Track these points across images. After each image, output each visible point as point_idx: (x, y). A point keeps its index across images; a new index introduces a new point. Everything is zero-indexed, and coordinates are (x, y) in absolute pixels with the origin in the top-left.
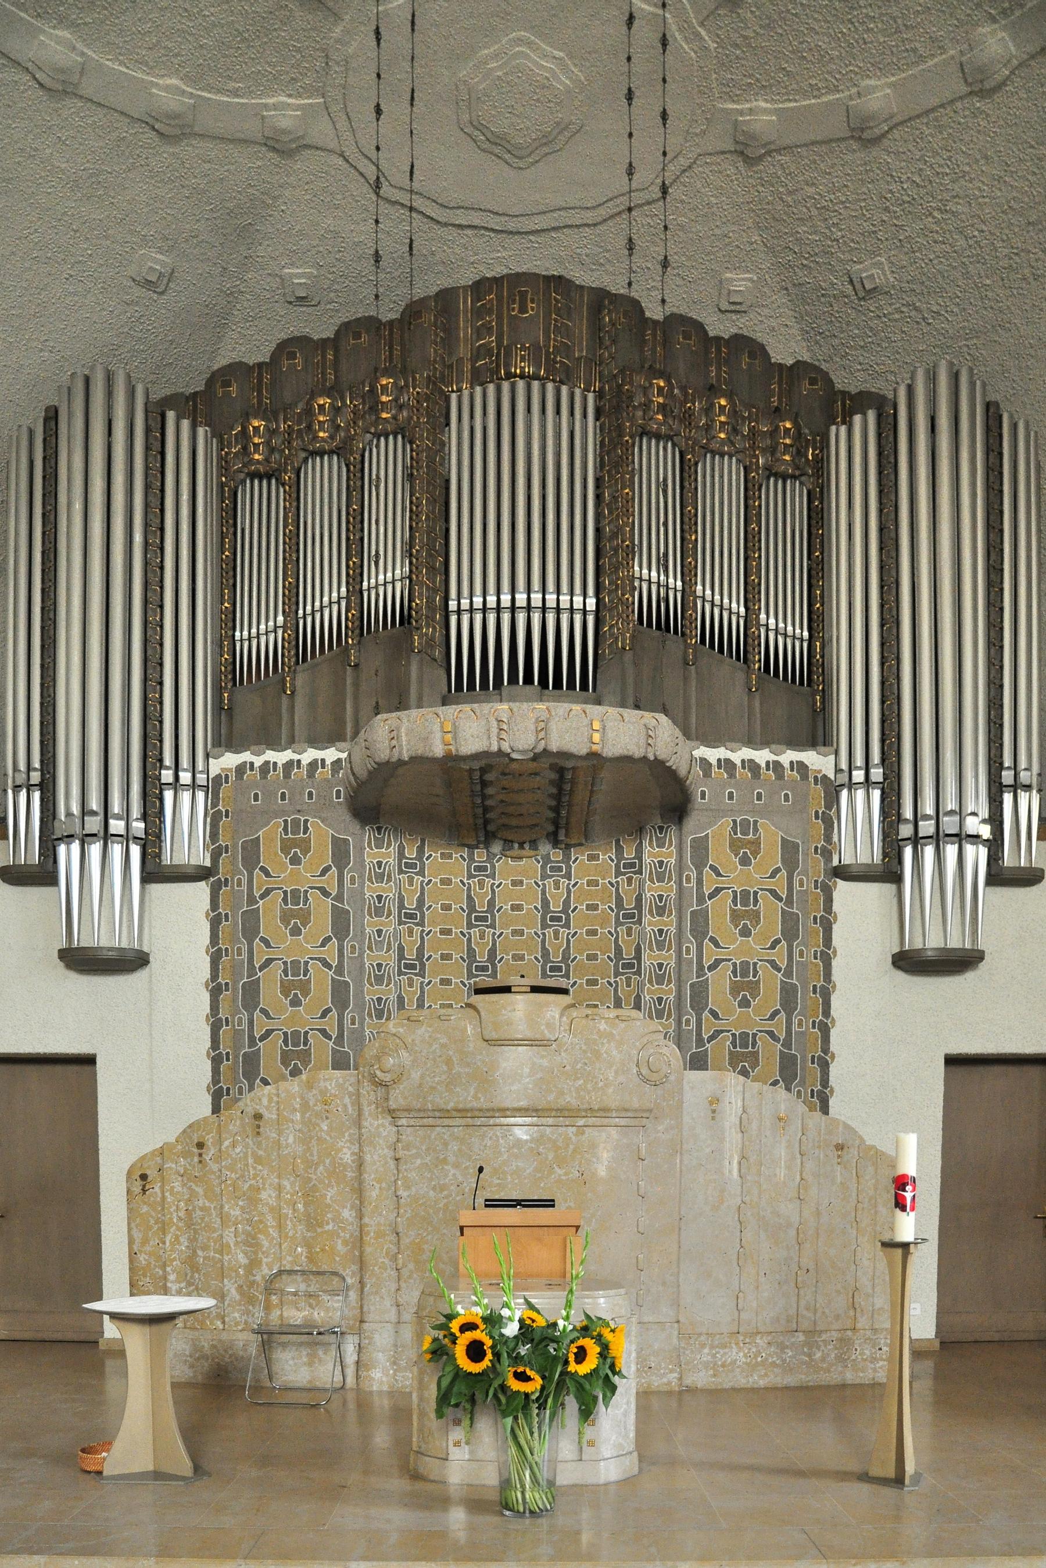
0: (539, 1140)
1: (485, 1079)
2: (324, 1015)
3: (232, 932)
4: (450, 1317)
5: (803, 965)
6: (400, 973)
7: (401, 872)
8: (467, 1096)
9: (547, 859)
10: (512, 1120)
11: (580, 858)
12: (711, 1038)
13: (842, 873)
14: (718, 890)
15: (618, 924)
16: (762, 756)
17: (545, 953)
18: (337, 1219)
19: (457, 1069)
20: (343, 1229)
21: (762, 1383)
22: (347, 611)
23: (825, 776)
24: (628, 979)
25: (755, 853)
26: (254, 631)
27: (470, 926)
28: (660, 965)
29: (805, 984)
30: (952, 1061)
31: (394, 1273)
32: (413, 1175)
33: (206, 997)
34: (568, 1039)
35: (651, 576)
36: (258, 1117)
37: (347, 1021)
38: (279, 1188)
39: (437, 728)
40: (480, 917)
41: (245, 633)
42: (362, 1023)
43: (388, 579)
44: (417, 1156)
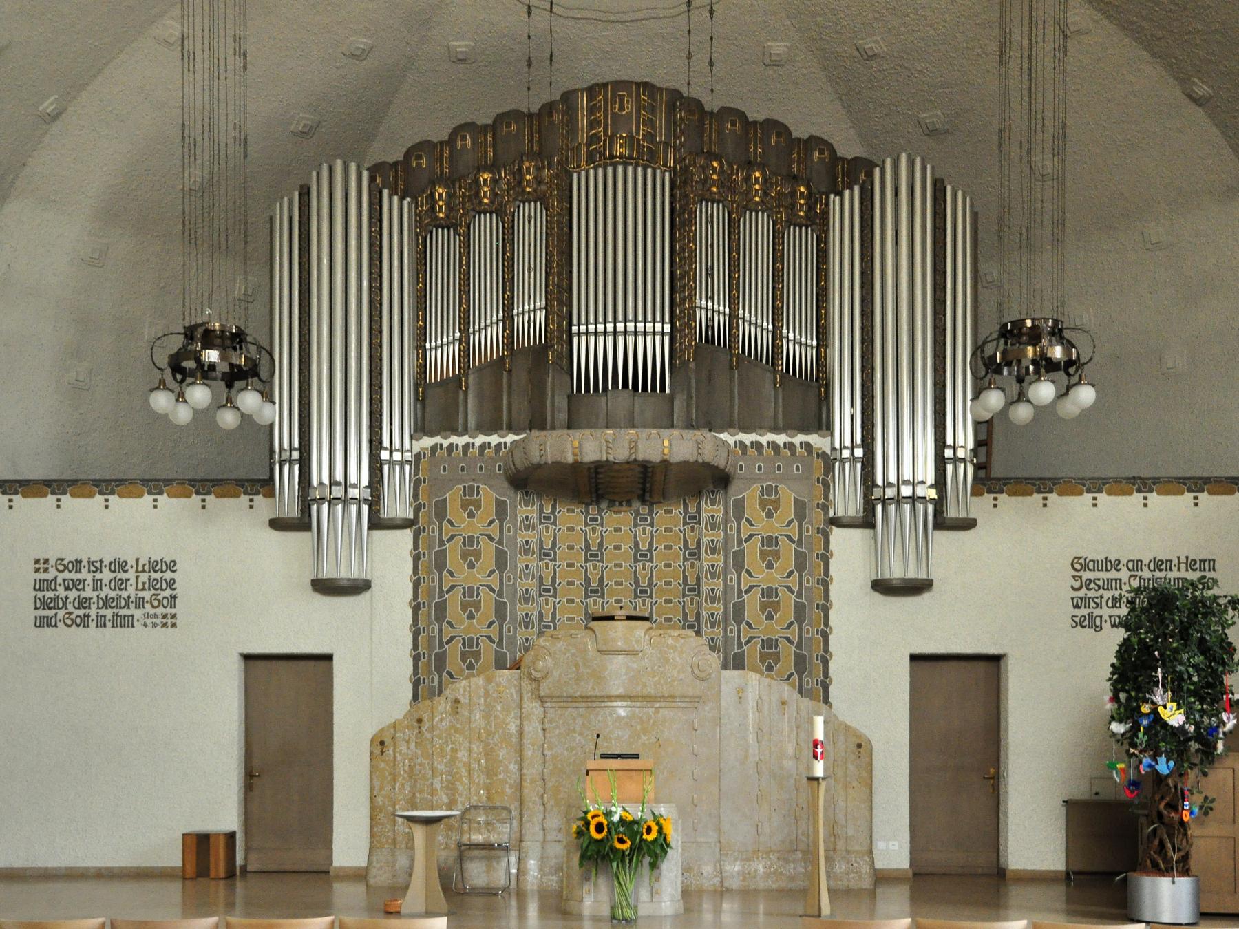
0: (631, 717)
1: (598, 676)
2: (489, 626)
3: (428, 565)
4: (586, 813)
5: (810, 588)
6: (541, 595)
7: (541, 523)
8: (588, 688)
9: (637, 513)
10: (615, 704)
11: (660, 512)
12: (748, 642)
13: (836, 522)
14: (751, 536)
15: (685, 559)
16: (781, 439)
17: (637, 581)
18: (507, 771)
19: (582, 670)
20: (510, 777)
21: (774, 886)
22: (504, 331)
23: (824, 453)
24: (692, 600)
25: (776, 509)
26: (439, 342)
27: (586, 560)
28: (713, 590)
29: (811, 603)
30: (914, 658)
31: (541, 808)
32: (553, 740)
33: (410, 612)
34: (649, 651)
35: (710, 308)
36: (457, 701)
37: (505, 630)
38: (470, 750)
39: (569, 446)
40: (593, 554)
41: (433, 344)
42: (515, 633)
43: (532, 315)
44: (557, 727)
